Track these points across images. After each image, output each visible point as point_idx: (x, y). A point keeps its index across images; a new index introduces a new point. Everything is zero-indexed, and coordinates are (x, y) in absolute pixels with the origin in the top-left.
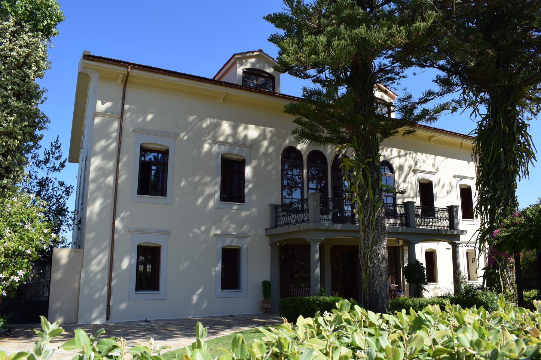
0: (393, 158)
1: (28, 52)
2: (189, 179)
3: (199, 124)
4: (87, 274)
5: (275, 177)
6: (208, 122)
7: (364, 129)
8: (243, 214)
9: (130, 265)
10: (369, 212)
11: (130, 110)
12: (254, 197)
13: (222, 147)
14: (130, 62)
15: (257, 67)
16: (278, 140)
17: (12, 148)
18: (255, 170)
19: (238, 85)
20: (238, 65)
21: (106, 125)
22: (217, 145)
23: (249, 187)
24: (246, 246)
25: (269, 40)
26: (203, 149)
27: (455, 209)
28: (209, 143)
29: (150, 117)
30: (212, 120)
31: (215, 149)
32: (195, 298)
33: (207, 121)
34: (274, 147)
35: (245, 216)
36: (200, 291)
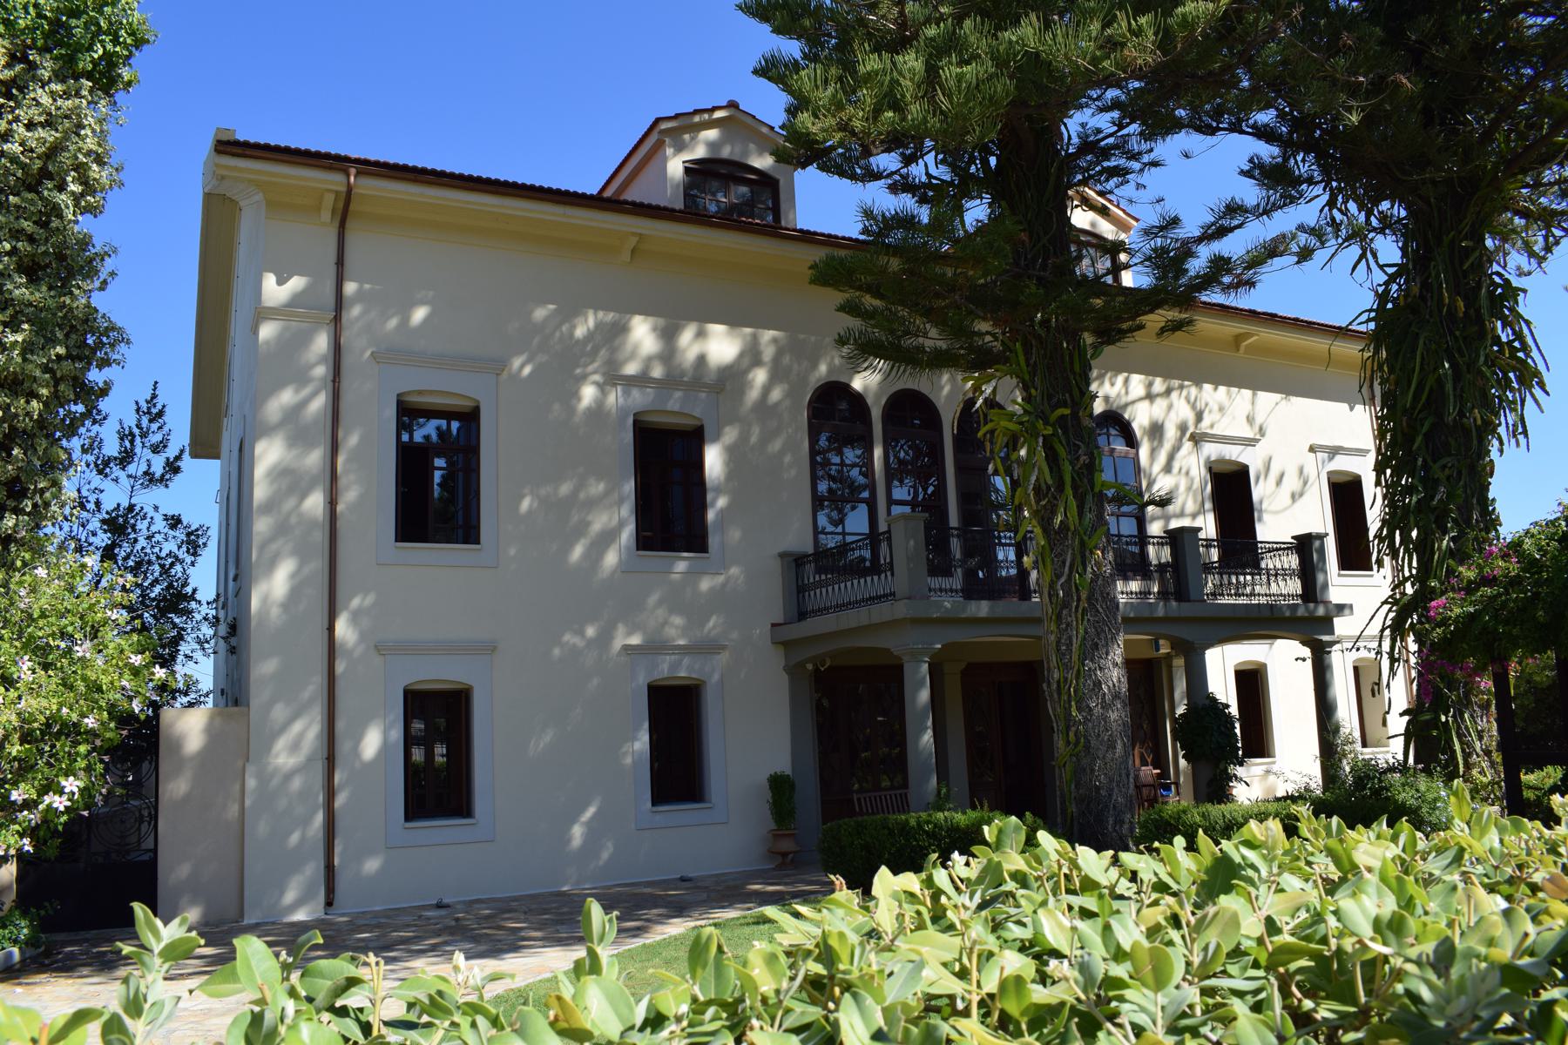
0: (1133, 402)
1: (52, 139)
3: (565, 328)
4: (263, 778)
5: (793, 472)
6: (591, 322)
7: (1045, 323)
8: (705, 584)
9: (385, 748)
10: (1068, 564)
11: (360, 296)
12: (735, 535)
13: (636, 393)
14: (354, 155)
15: (726, 153)
19: (673, 210)
20: (669, 151)
21: (292, 344)
22: (619, 388)
23: (718, 505)
24: (716, 677)
25: (755, 72)
26: (579, 399)
27: (1317, 544)
28: (596, 383)
29: (419, 314)
30: (601, 314)
31: (614, 398)
32: (577, 832)
33: (586, 321)
34: (786, 386)
35: (712, 589)
36: (590, 812)
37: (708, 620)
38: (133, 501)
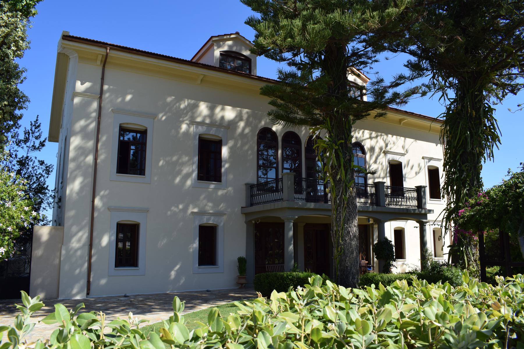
0: (365, 139)
1: (7, 31)
3: (177, 104)
4: (68, 251)
5: (251, 157)
6: (186, 103)
7: (337, 112)
8: (220, 193)
9: (110, 242)
10: (341, 192)
11: (109, 90)
12: (231, 177)
13: (200, 128)
14: (109, 43)
15: (234, 49)
18: (232, 151)
19: (216, 67)
20: (215, 48)
21: (85, 105)
22: (194, 126)
23: (225, 166)
24: (222, 224)
25: (245, 23)
26: (181, 129)
28: (187, 124)
29: (129, 97)
30: (190, 101)
31: (192, 129)
32: (173, 273)
33: (185, 102)
34: (250, 128)
35: (222, 195)
36: (178, 267)
38: (28, 155)
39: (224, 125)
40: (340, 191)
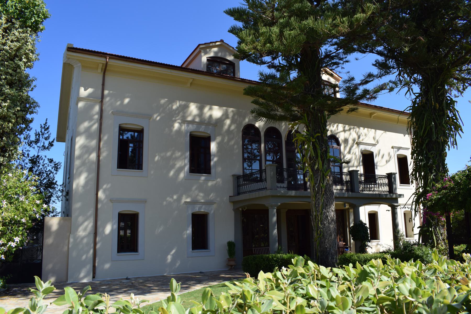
0: (339, 132)
1: (18, 45)
2: (162, 155)
3: (170, 106)
4: (75, 239)
5: (237, 151)
6: (178, 104)
7: (313, 108)
8: (210, 184)
10: (319, 180)
11: (109, 95)
14: (108, 53)
15: (219, 55)
16: (239, 119)
17: (7, 130)
18: (220, 145)
19: (203, 72)
20: (202, 54)
21: (88, 108)
23: (214, 160)
24: (212, 212)
25: (229, 31)
26: (174, 127)
27: (393, 176)
28: (179, 123)
29: (127, 101)
30: (181, 102)
31: (184, 127)
32: (169, 257)
33: (176, 104)
34: (236, 125)
35: (212, 186)
36: (173, 251)
37: (210, 195)
39: (212, 122)
40: (318, 180)
